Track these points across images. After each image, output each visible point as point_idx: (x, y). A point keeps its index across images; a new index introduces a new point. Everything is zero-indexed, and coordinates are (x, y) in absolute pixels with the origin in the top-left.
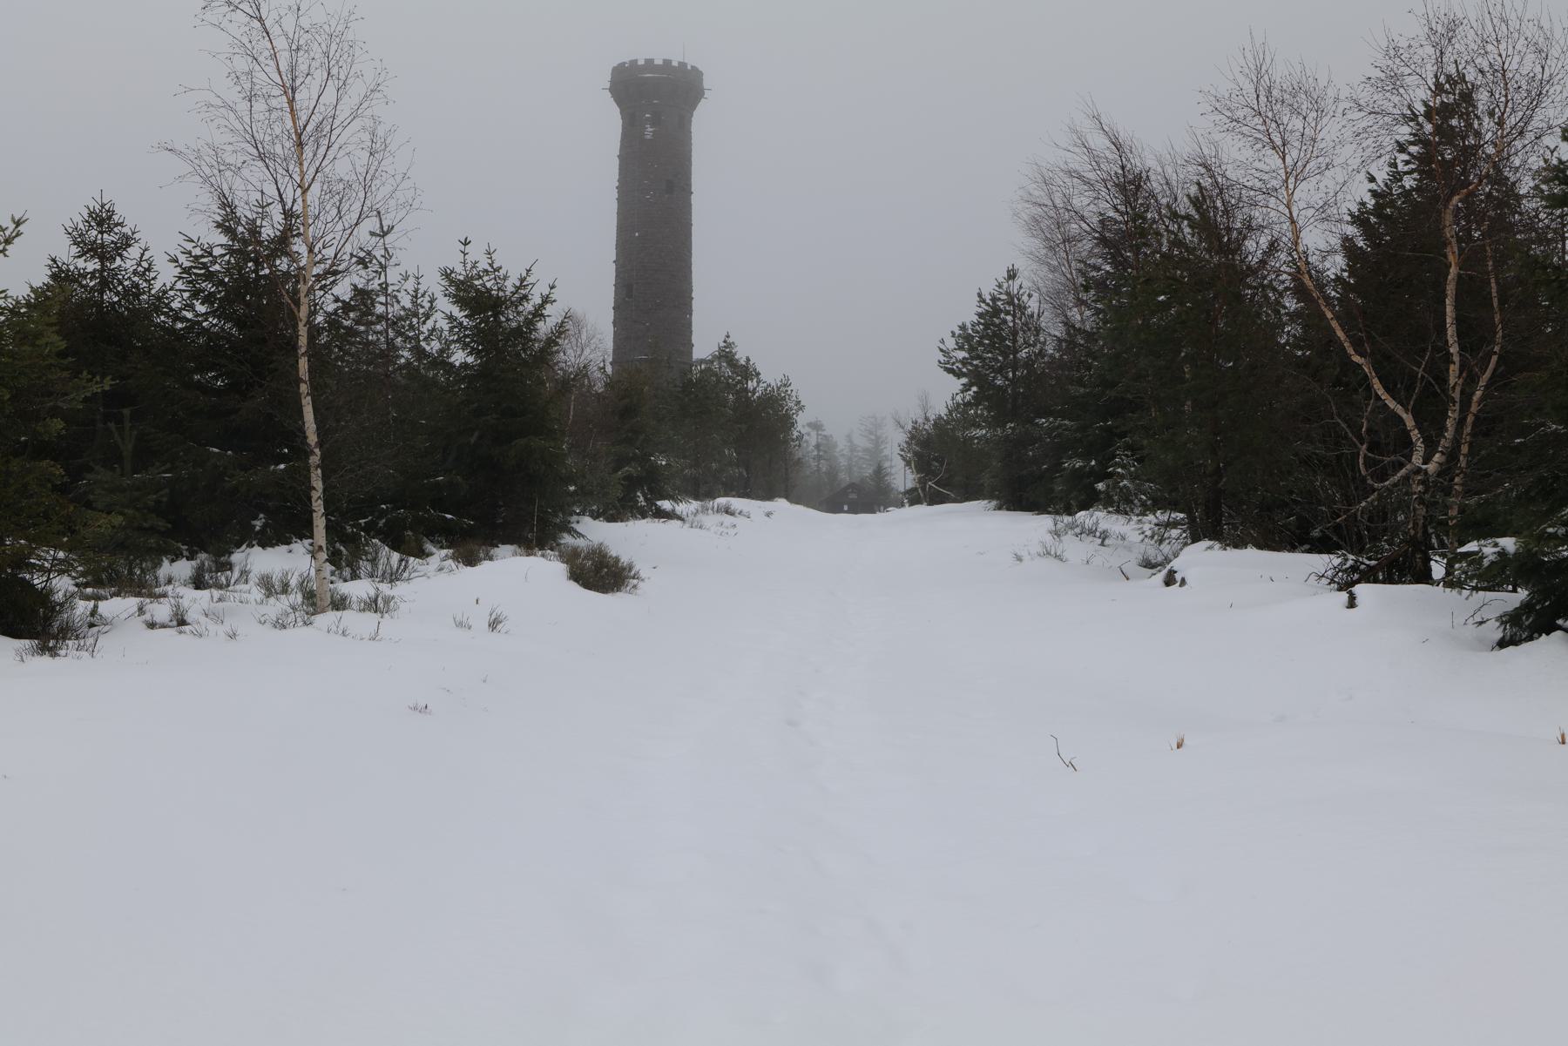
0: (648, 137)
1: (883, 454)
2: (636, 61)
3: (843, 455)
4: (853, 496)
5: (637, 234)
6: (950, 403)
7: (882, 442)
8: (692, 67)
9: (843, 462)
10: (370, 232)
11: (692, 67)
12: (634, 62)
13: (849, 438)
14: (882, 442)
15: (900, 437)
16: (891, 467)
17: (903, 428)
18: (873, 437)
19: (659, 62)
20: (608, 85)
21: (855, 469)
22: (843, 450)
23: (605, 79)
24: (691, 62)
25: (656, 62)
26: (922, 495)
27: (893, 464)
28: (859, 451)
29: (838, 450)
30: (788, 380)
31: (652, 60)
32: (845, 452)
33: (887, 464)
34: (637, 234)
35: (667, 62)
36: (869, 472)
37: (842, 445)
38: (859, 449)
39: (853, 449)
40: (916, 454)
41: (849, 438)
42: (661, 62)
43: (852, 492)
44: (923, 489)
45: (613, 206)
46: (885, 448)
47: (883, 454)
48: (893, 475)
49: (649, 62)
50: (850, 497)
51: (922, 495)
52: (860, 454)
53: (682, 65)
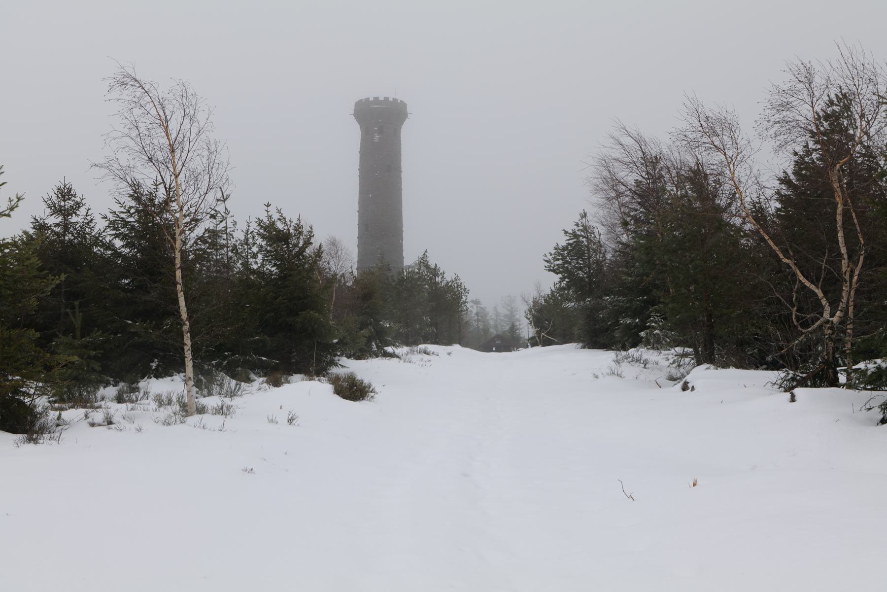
1: (515, 318)
3: (492, 319)
4: (498, 342)
5: (370, 196)
8: (400, 101)
9: (492, 323)
11: (400, 101)
13: (495, 309)
16: (520, 325)
19: (381, 98)
20: (353, 112)
23: (351, 109)
24: (400, 98)
26: (538, 340)
28: (501, 316)
31: (378, 98)
32: (493, 317)
33: (518, 323)
35: (386, 99)
36: (507, 328)
37: (491, 313)
38: (501, 315)
39: (497, 315)
41: (495, 309)
42: (383, 99)
44: (539, 337)
46: (517, 314)
47: (515, 318)
49: (376, 99)
51: (538, 340)
52: (502, 318)
53: (395, 100)
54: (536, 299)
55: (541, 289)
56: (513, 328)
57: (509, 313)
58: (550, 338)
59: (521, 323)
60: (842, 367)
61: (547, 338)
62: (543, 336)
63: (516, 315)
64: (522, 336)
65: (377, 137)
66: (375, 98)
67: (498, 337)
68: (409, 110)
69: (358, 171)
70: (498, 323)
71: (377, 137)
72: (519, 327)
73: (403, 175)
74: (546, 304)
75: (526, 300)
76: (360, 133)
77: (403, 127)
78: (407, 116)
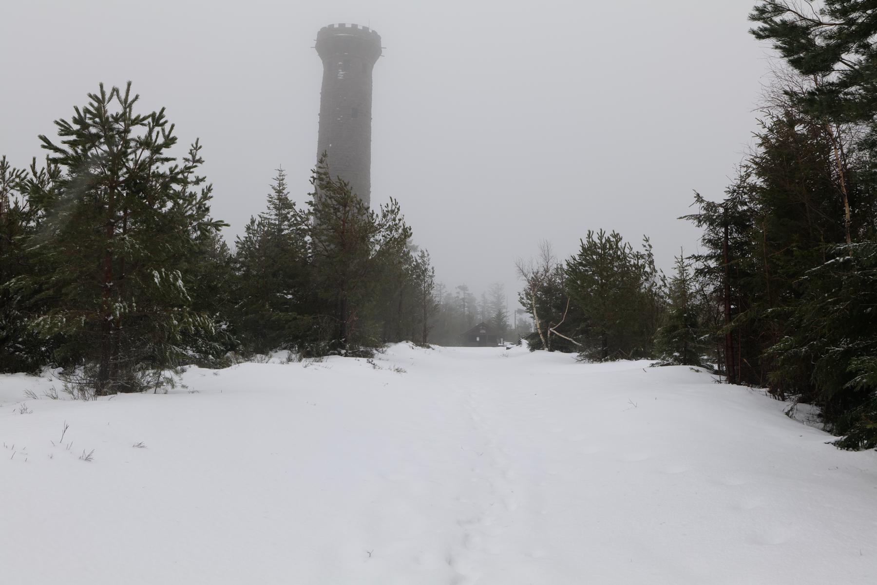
0: (340, 78)
1: (502, 305)
2: (333, 25)
3: (480, 305)
4: (483, 331)
5: (330, 145)
6: (585, 242)
7: (502, 298)
8: (372, 31)
9: (479, 309)
10: (184, 159)
11: (372, 31)
12: (331, 26)
14: (502, 298)
15: (523, 285)
16: (507, 312)
17: (526, 276)
18: (496, 295)
19: (348, 26)
20: (314, 43)
21: (486, 313)
22: (480, 302)
23: (312, 39)
24: (372, 27)
25: (347, 26)
26: (543, 340)
27: (508, 310)
29: (476, 302)
30: (396, 204)
31: (344, 24)
32: (481, 304)
33: (504, 310)
34: (330, 145)
35: (354, 26)
36: (494, 315)
37: (479, 300)
38: (489, 302)
40: (538, 300)
42: (350, 26)
43: (483, 329)
44: (545, 334)
45: (317, 127)
46: (503, 301)
47: (502, 305)
48: (507, 317)
49: (342, 26)
50: (481, 332)
51: (543, 340)
52: (490, 305)
53: (365, 29)
54: (537, 273)
55: (551, 255)
56: (500, 316)
57: (496, 300)
58: (563, 336)
59: (508, 310)
60: (555, 326)
61: (559, 336)
62: (552, 333)
63: (503, 303)
64: (508, 323)
65: (341, 73)
66: (340, 25)
67: (483, 325)
68: (383, 44)
69: (319, 117)
70: (485, 310)
71: (341, 73)
72: (505, 314)
73: (373, 124)
74: (768, 150)
75: (525, 271)
76: (322, 69)
77: (376, 66)
78: (381, 53)
